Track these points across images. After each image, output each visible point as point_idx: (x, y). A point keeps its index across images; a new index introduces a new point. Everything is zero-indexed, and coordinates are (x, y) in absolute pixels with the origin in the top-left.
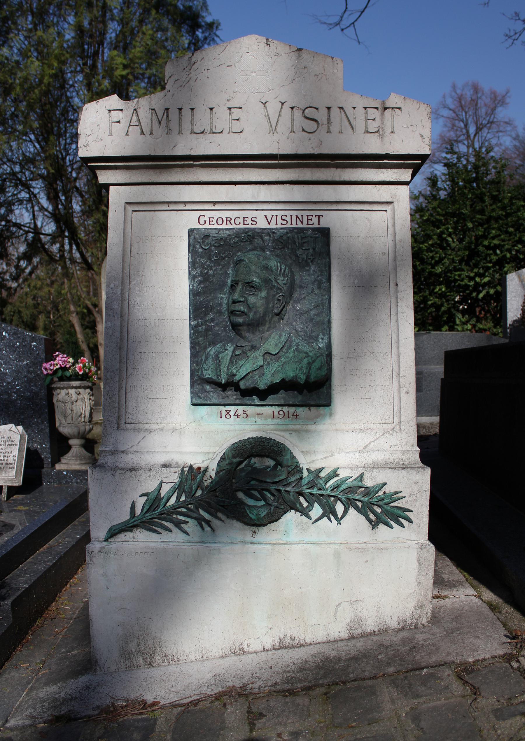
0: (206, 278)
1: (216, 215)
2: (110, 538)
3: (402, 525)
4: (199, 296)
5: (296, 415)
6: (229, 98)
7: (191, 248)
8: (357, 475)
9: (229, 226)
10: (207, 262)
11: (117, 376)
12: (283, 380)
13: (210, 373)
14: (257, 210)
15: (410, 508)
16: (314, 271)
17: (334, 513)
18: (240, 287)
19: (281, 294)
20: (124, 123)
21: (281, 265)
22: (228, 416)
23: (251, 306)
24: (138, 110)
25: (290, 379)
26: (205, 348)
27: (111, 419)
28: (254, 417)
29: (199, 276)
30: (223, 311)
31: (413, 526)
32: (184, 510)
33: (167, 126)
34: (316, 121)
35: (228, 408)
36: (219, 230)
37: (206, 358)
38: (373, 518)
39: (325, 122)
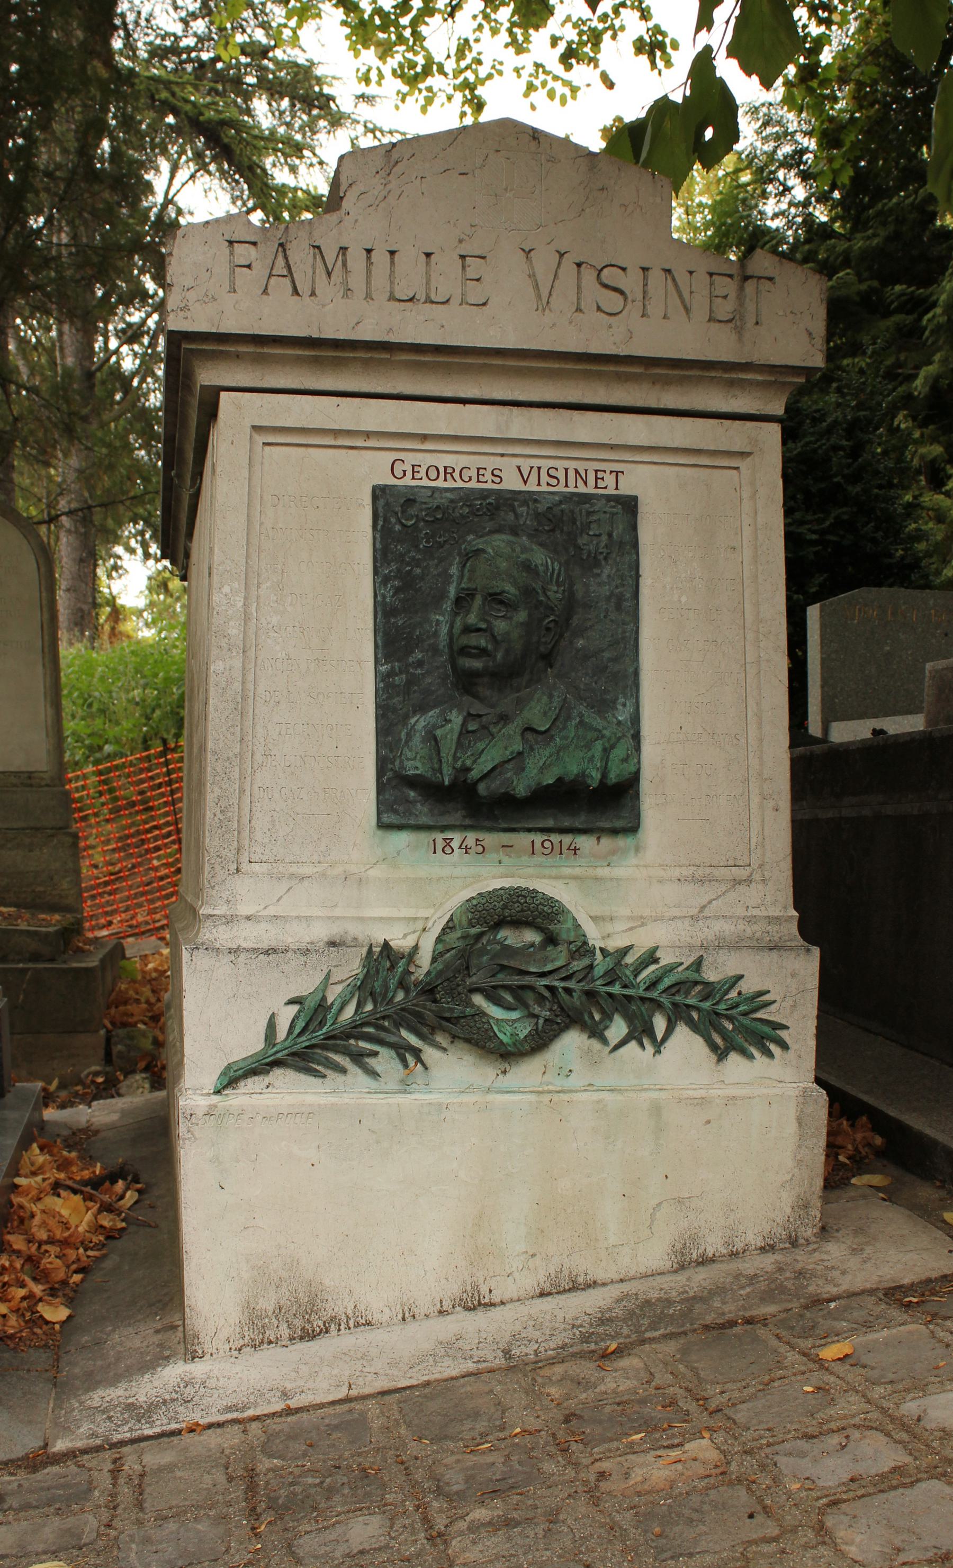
0: (407, 583)
1: (427, 460)
2: (225, 1087)
3: (770, 1055)
4: (395, 617)
5: (575, 849)
6: (463, 236)
7: (381, 523)
8: (691, 960)
9: (450, 484)
10: (409, 551)
11: (237, 769)
12: (560, 780)
13: (419, 765)
14: (502, 455)
15: (784, 1022)
16: (609, 576)
17: (649, 1031)
18: (478, 601)
19: (552, 618)
20: (259, 270)
22: (448, 850)
23: (499, 638)
24: (288, 246)
25: (572, 777)
26: (407, 717)
27: (224, 853)
28: (497, 852)
29: (395, 577)
30: (441, 647)
31: (791, 1054)
32: (371, 1030)
33: (345, 282)
34: (621, 292)
35: (449, 835)
36: (434, 490)
37: (409, 736)
38: (718, 1040)
39: (640, 296)
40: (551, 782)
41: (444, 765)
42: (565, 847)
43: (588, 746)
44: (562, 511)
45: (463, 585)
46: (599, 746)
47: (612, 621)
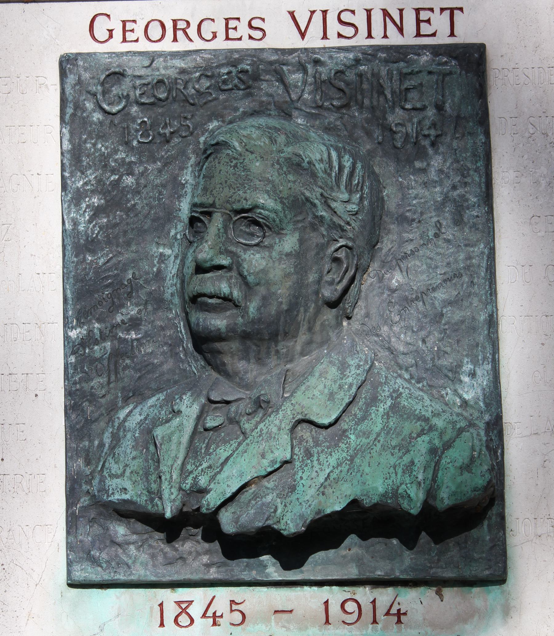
0: (114, 199)
4: (93, 252)
5: (399, 614)
7: (70, 111)
9: (183, 45)
10: (116, 151)
12: (354, 503)
13: (128, 485)
19: (342, 242)
21: (340, 157)
22: (184, 620)
23: (251, 279)
25: (376, 499)
26: (113, 408)
30: (167, 296)
35: (183, 594)
36: (153, 56)
37: (116, 439)
40: (338, 508)
41: (165, 486)
44: (360, 75)
45: (196, 200)
47: (448, 241)
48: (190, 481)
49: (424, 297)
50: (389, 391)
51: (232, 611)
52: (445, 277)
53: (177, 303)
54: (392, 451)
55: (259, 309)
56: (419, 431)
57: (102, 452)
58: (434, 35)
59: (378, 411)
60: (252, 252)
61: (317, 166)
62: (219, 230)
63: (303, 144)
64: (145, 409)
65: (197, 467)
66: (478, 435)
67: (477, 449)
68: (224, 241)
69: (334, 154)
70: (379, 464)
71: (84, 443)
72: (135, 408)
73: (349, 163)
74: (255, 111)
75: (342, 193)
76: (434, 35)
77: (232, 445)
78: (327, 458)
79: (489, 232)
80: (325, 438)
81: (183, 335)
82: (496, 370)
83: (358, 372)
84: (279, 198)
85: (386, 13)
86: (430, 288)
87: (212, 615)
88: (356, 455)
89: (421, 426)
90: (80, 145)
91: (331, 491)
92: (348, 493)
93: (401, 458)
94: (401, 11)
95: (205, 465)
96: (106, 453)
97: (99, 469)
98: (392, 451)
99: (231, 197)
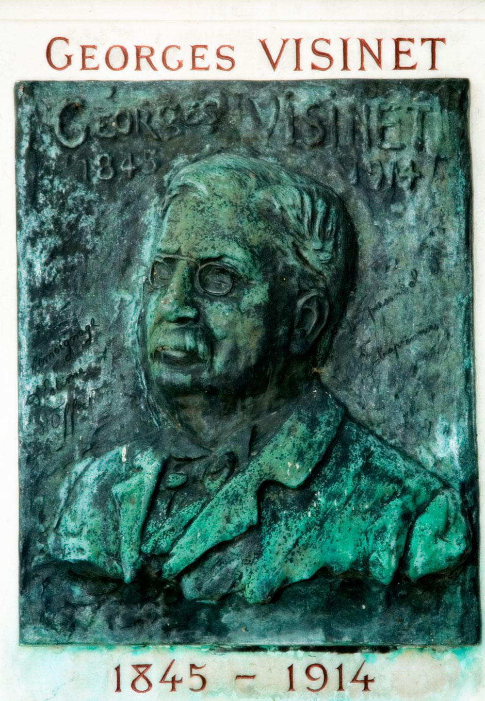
0: (66, 244)
9: (146, 75)
10: (74, 189)
13: (85, 544)
19: (314, 293)
21: (313, 202)
22: (141, 684)
25: (346, 566)
26: (68, 462)
30: (128, 344)
36: (115, 88)
42: (347, 676)
43: (376, 511)
45: (159, 245)
46: (394, 509)
48: (151, 543)
49: (398, 349)
50: (360, 450)
51: (192, 675)
52: (421, 329)
53: (138, 351)
54: (364, 516)
55: (226, 363)
56: (392, 494)
57: (58, 508)
58: (413, 67)
59: (348, 471)
60: (219, 303)
61: (289, 212)
62: (184, 279)
63: (275, 187)
64: (103, 464)
65: (159, 529)
66: (453, 498)
67: (452, 514)
68: (190, 291)
69: (307, 199)
70: (350, 529)
71: (38, 498)
72: (92, 462)
73: (323, 208)
74: (222, 148)
75: (315, 241)
76: (413, 67)
77: (195, 506)
78: (295, 522)
79: (468, 282)
80: (293, 501)
81: (143, 386)
82: (472, 428)
83: (328, 429)
84: (249, 247)
85: (363, 43)
86: (405, 340)
87: (171, 680)
88: (326, 519)
89: (394, 488)
90: (36, 181)
91: (299, 557)
92: (317, 560)
93: (373, 523)
94: (379, 41)
95: (167, 527)
96: (62, 510)
97: (54, 526)
98: (364, 516)
99: (197, 245)
